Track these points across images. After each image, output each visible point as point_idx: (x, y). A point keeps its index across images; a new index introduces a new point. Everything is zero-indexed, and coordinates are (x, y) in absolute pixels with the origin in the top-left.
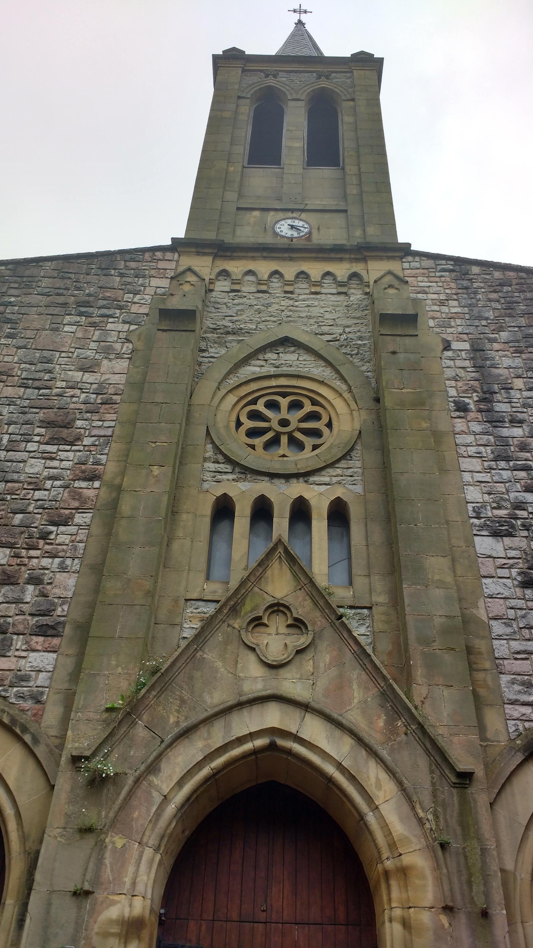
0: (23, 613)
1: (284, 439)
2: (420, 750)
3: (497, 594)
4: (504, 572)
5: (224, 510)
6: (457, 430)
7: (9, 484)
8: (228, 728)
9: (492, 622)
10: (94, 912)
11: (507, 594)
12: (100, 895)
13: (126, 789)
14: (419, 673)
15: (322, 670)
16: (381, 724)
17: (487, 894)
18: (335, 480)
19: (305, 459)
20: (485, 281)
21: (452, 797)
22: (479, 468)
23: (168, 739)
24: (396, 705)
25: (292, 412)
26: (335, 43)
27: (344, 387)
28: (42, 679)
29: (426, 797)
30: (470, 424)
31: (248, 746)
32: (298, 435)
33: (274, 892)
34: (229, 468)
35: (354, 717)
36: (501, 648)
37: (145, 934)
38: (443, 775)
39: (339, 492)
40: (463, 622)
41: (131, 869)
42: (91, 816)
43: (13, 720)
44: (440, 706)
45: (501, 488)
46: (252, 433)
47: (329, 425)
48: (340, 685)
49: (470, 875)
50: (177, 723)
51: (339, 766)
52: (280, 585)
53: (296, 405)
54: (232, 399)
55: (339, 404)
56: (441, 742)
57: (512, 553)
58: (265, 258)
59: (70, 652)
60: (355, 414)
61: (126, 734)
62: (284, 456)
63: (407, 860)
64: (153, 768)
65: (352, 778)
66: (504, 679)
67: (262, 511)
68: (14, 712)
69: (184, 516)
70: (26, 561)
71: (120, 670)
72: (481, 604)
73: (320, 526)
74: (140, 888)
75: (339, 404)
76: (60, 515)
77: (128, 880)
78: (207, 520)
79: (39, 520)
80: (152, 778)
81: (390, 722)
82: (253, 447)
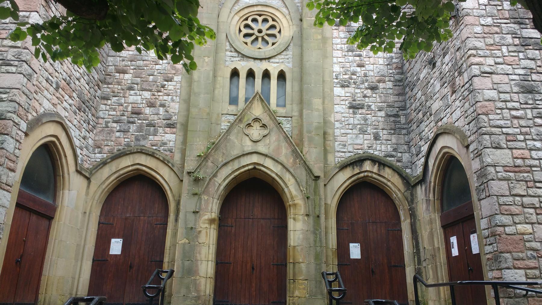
0: (160, 119)
1: (260, 39)
2: (304, 169)
4: (343, 103)
5: (235, 73)
6: (334, 36)
7: (144, 62)
8: (239, 162)
9: (336, 123)
10: (200, 217)
11: (343, 111)
12: (201, 213)
13: (207, 182)
14: (306, 144)
16: (291, 161)
17: (320, 211)
18: (281, 61)
19: (268, 50)
21: (312, 183)
22: (340, 56)
23: (219, 166)
24: (297, 154)
25: (264, 24)
27: (287, 12)
28: (172, 144)
29: (304, 184)
30: (340, 33)
31: (247, 168)
32: (266, 37)
33: (256, 209)
34: (235, 54)
35: (282, 159)
36: (337, 132)
37: (216, 223)
38: (310, 177)
39: (282, 67)
40: (324, 123)
41: (210, 205)
42: (196, 190)
43: (164, 159)
44: (312, 155)
45: (348, 65)
46: (246, 35)
47: (280, 32)
49: (315, 206)
50: (222, 161)
51: (277, 174)
52: (257, 110)
53: (265, 21)
54: (237, 18)
55: (284, 21)
56: (311, 167)
57: (348, 95)
59: (180, 134)
60: (291, 27)
61: (205, 165)
62: (260, 48)
63: (296, 202)
64: (215, 175)
65: (281, 178)
66: (337, 143)
67: (251, 74)
68: (164, 156)
69: (219, 78)
70: (158, 97)
71: (200, 143)
72: (333, 115)
73: (274, 82)
74: (214, 210)
75: (284, 21)
76: (168, 77)
77: (210, 208)
78: (229, 79)
79: (160, 79)
80: (215, 178)
81: (295, 160)
82: (246, 43)
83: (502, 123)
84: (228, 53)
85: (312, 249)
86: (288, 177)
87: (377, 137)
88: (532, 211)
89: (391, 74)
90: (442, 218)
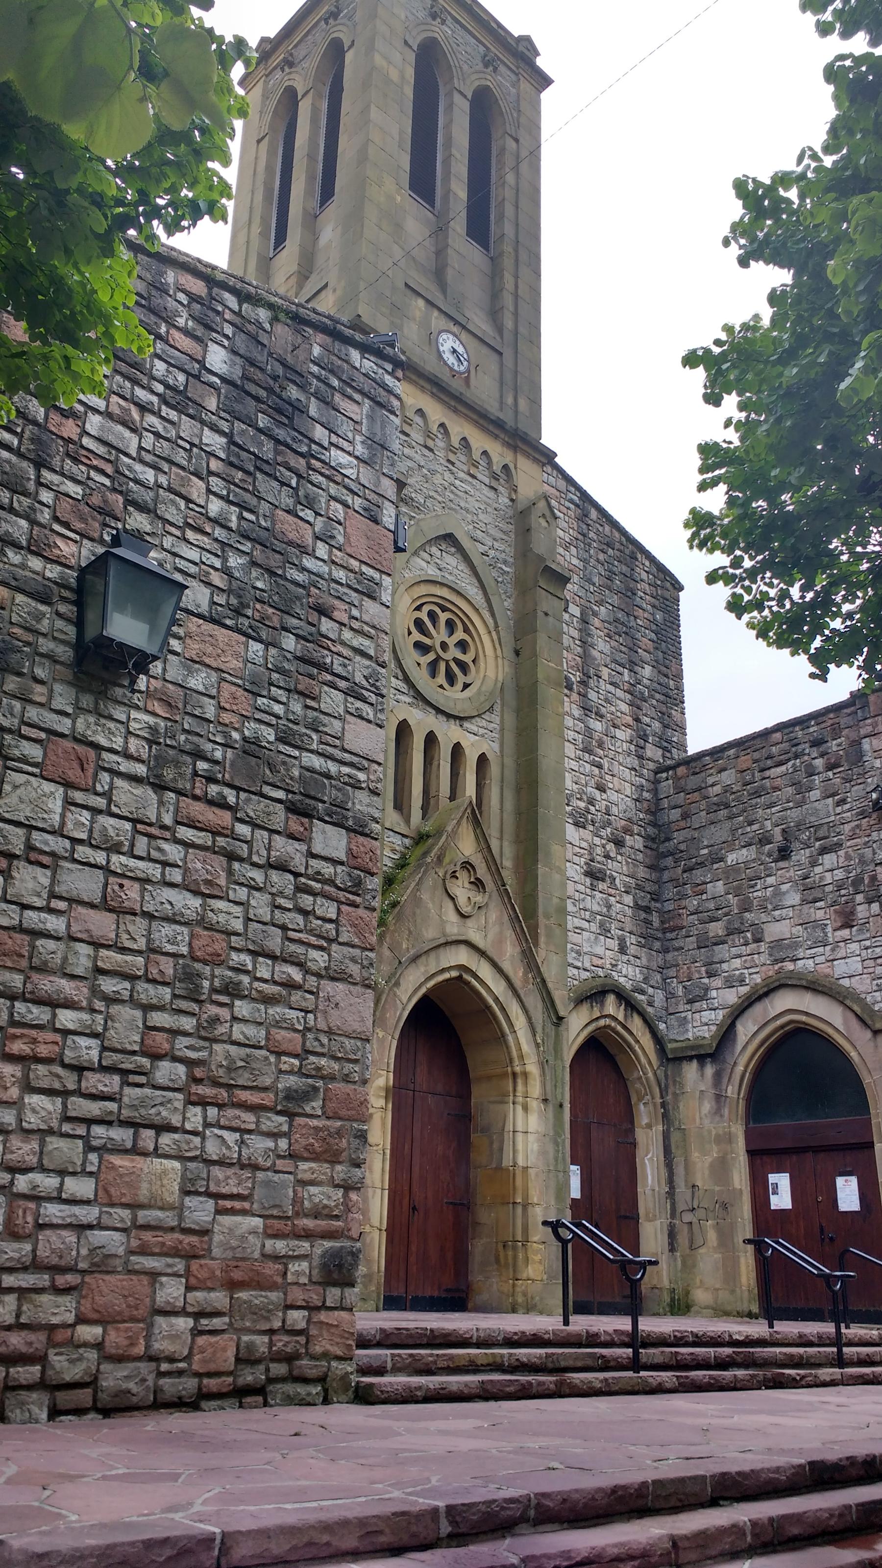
1: (431, 656)
8: (438, 959)
15: (490, 925)
17: (563, 1094)
18: (482, 731)
26: (735, 210)
31: (447, 976)
32: (442, 666)
35: (506, 966)
48: (500, 941)
58: (433, 395)
65: (503, 1009)
81: (525, 974)
85: (551, 1175)
86: (514, 1009)
87: (623, 950)
89: (641, 820)
90: (749, 1136)
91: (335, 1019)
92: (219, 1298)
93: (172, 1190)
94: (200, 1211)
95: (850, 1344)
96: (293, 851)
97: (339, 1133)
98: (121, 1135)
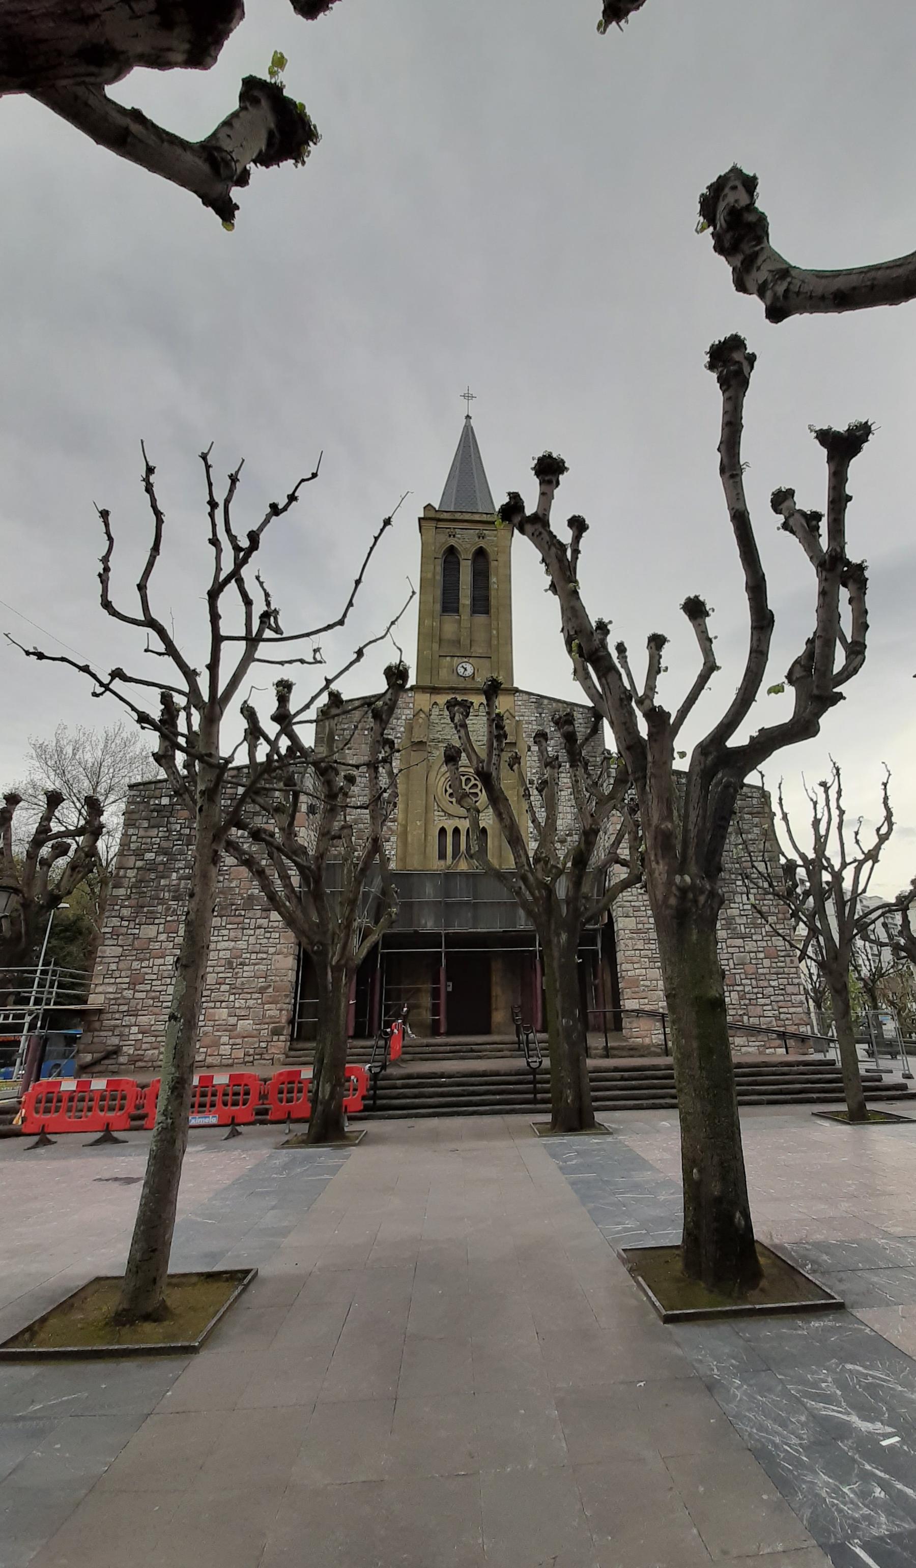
3: (839, 807)
5: (443, 831)
20: (549, 709)
34: (443, 814)
54: (443, 779)
82: (452, 802)
83: (630, 898)
84: (436, 813)
88: (646, 960)
91: (278, 966)
92: (239, 1041)
93: (225, 1016)
94: (232, 1020)
95: (539, 1083)
96: (264, 922)
97: (279, 996)
98: (212, 1005)
